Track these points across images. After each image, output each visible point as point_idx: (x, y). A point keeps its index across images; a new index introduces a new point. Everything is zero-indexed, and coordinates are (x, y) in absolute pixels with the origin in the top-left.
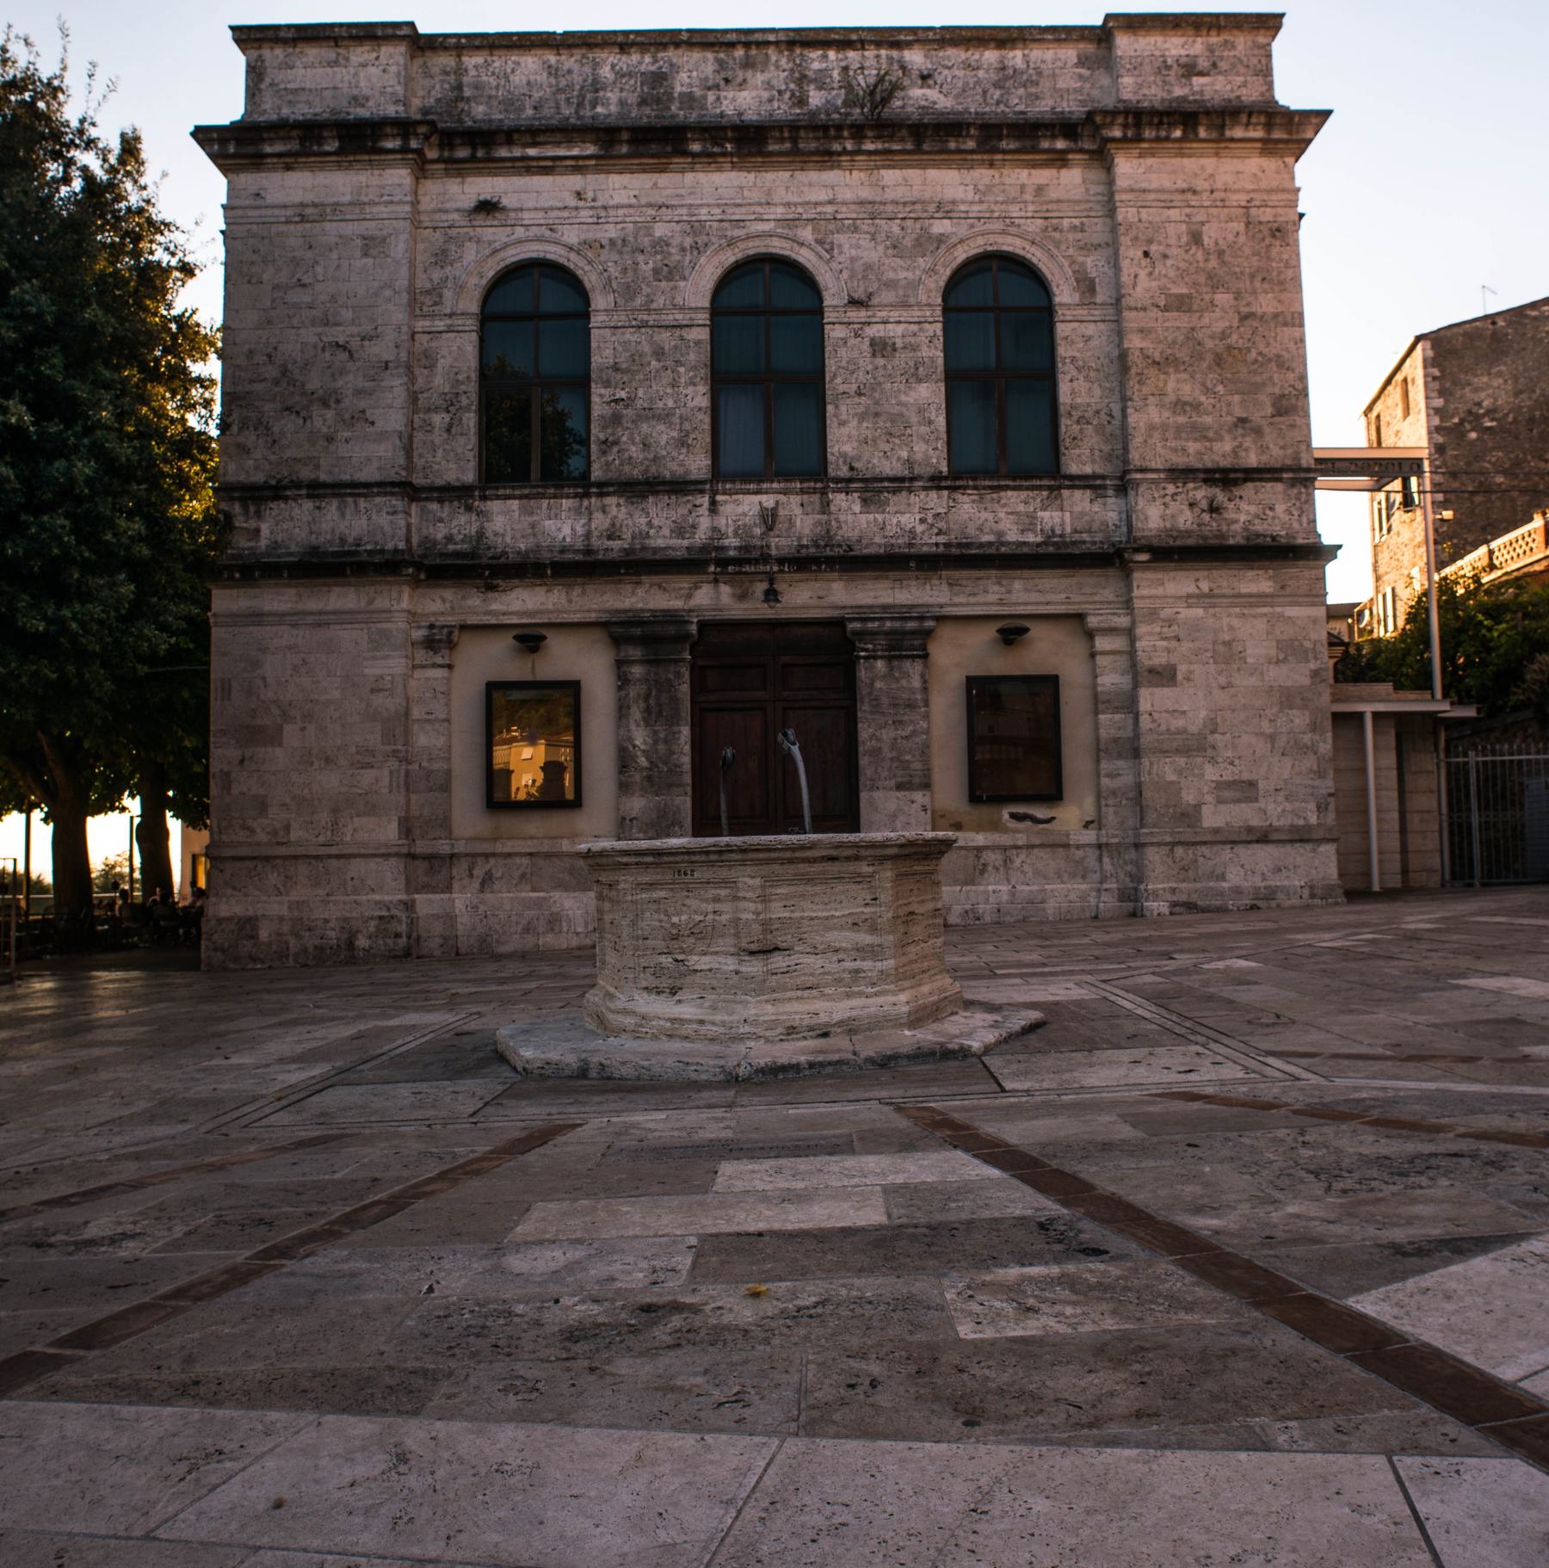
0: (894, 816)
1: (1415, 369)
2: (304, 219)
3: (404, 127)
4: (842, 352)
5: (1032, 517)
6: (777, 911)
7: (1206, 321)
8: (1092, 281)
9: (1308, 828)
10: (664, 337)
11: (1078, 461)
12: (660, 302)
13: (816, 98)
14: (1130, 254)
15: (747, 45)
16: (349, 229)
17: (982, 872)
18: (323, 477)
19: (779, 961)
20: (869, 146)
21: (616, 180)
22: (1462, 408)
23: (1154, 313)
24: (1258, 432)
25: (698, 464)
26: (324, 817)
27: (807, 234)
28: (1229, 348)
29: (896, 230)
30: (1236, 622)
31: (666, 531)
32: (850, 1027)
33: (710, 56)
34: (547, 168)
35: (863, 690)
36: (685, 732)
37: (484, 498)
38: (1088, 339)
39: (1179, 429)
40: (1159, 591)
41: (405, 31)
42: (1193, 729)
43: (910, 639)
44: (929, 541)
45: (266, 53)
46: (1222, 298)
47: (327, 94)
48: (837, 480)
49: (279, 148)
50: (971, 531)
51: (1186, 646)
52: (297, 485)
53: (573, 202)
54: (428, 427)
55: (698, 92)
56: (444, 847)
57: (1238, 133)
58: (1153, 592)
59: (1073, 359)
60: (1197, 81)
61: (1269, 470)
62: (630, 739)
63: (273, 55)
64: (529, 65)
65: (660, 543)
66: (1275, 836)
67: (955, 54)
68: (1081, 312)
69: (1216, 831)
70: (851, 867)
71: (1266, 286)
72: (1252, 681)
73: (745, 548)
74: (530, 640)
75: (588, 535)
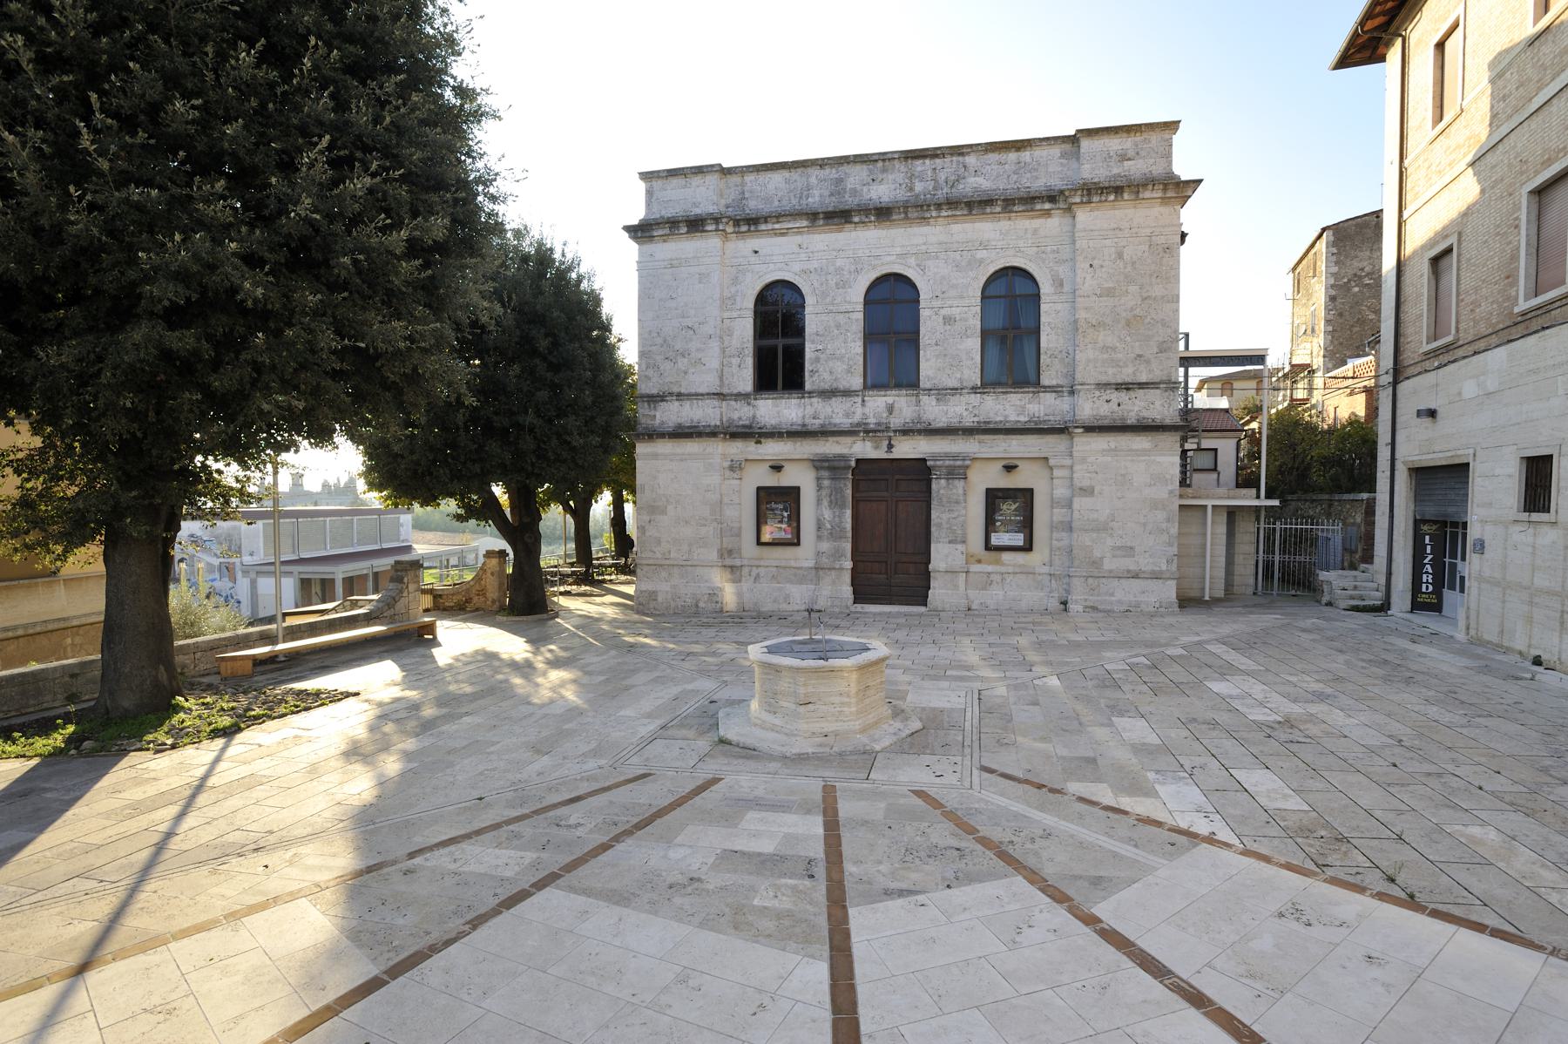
1: (1322, 246)
5: (1023, 407)
9: (1161, 572)
10: (841, 318)
12: (839, 300)
13: (919, 187)
14: (1082, 265)
22: (1350, 272)
24: (1148, 362)
25: (857, 382)
27: (912, 261)
35: (934, 494)
36: (849, 512)
43: (958, 472)
44: (969, 421)
46: (1133, 289)
52: (671, 394)
56: (738, 562)
57: (1147, 194)
63: (657, 184)
68: (1055, 298)
73: (878, 424)
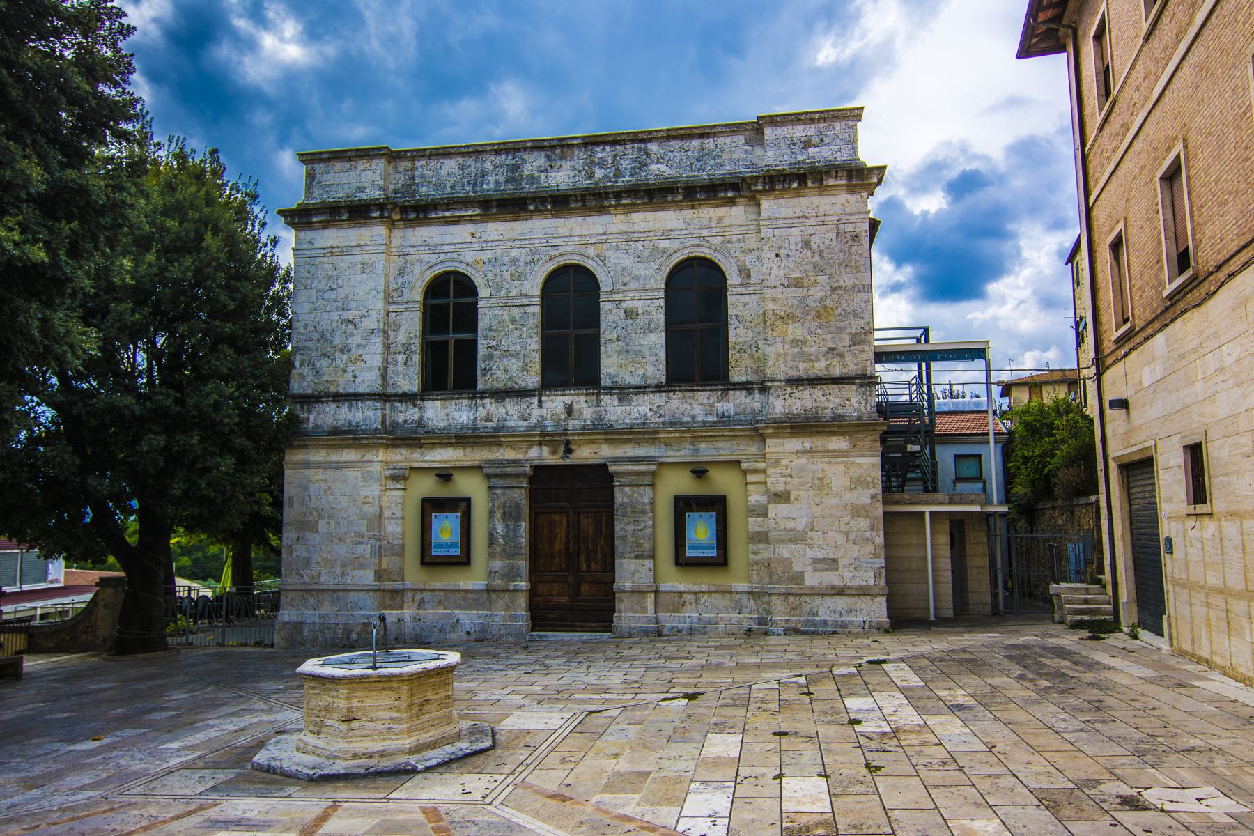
0: (633, 574)
2: (332, 255)
3: (381, 206)
4: (610, 317)
5: (712, 406)
6: (355, 703)
7: (811, 292)
8: (749, 271)
9: (868, 587)
10: (515, 312)
11: (737, 375)
13: (599, 174)
15: (562, 146)
16: (359, 258)
17: (683, 605)
18: (341, 390)
19: (355, 724)
20: (624, 202)
21: (492, 226)
23: (781, 289)
24: (841, 355)
25: (532, 380)
26: (338, 570)
28: (825, 307)
29: (640, 247)
30: (826, 467)
31: (515, 417)
32: (382, 754)
33: (543, 154)
34: (456, 221)
37: (423, 400)
38: (745, 304)
39: (794, 356)
40: (780, 449)
41: (384, 152)
42: (800, 528)
45: (316, 166)
47: (346, 186)
48: (605, 388)
49: (320, 218)
50: (678, 415)
51: (796, 480)
52: (328, 395)
53: (470, 239)
54: (396, 363)
55: (536, 174)
57: (831, 182)
58: (777, 450)
59: (737, 316)
60: (811, 150)
61: (847, 378)
62: (495, 529)
64: (450, 165)
65: (512, 423)
66: (848, 592)
67: (676, 144)
69: (812, 588)
70: (389, 684)
71: (848, 270)
72: (836, 501)
74: (445, 476)
75: (475, 419)
